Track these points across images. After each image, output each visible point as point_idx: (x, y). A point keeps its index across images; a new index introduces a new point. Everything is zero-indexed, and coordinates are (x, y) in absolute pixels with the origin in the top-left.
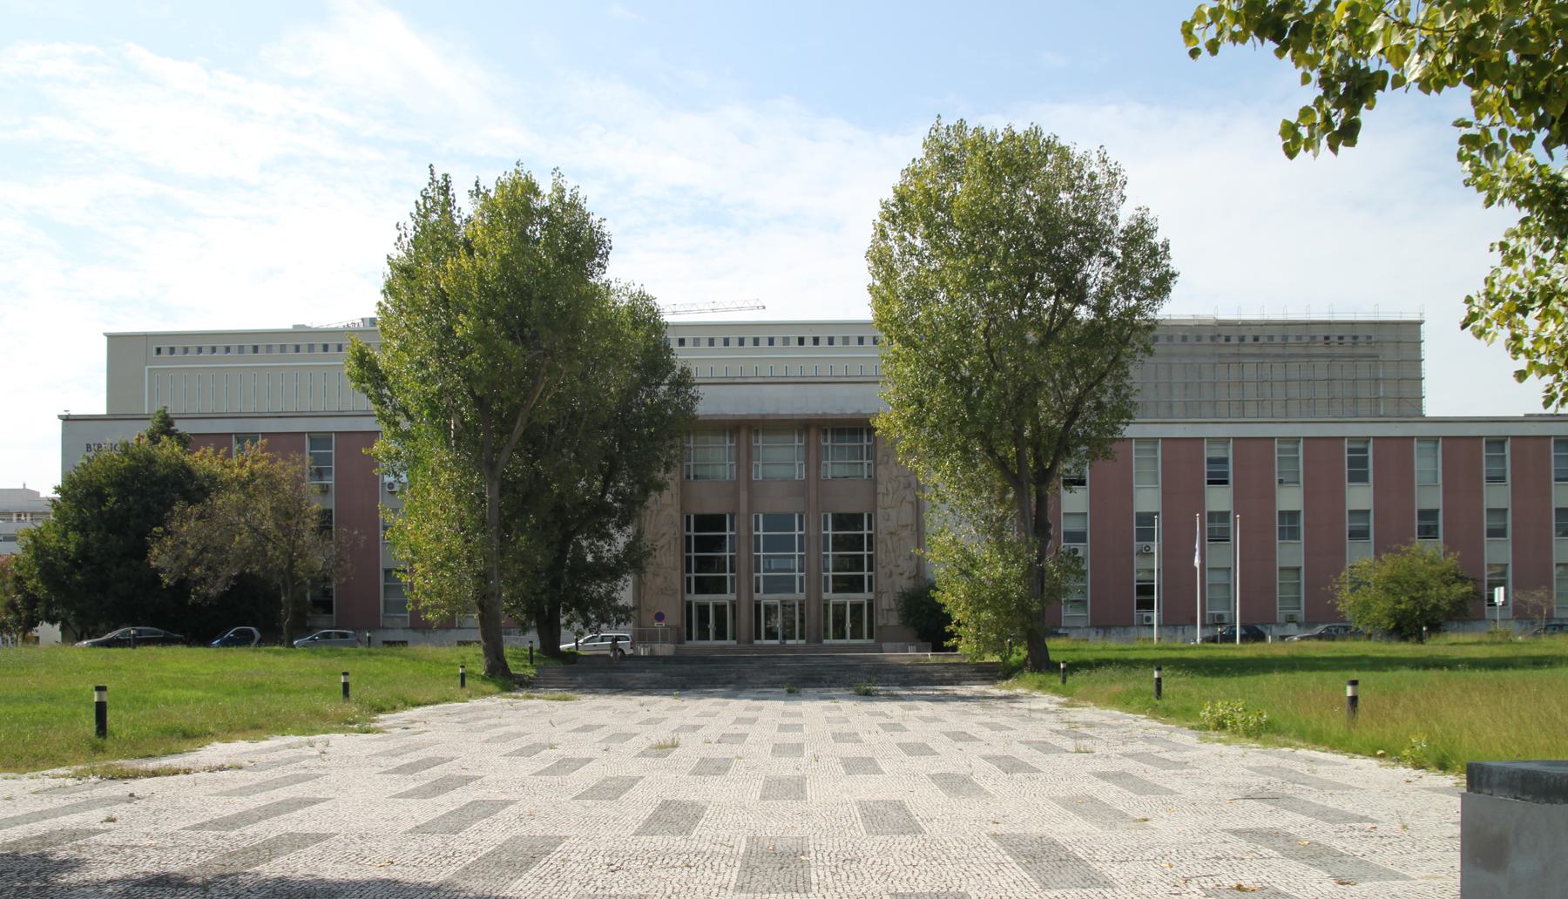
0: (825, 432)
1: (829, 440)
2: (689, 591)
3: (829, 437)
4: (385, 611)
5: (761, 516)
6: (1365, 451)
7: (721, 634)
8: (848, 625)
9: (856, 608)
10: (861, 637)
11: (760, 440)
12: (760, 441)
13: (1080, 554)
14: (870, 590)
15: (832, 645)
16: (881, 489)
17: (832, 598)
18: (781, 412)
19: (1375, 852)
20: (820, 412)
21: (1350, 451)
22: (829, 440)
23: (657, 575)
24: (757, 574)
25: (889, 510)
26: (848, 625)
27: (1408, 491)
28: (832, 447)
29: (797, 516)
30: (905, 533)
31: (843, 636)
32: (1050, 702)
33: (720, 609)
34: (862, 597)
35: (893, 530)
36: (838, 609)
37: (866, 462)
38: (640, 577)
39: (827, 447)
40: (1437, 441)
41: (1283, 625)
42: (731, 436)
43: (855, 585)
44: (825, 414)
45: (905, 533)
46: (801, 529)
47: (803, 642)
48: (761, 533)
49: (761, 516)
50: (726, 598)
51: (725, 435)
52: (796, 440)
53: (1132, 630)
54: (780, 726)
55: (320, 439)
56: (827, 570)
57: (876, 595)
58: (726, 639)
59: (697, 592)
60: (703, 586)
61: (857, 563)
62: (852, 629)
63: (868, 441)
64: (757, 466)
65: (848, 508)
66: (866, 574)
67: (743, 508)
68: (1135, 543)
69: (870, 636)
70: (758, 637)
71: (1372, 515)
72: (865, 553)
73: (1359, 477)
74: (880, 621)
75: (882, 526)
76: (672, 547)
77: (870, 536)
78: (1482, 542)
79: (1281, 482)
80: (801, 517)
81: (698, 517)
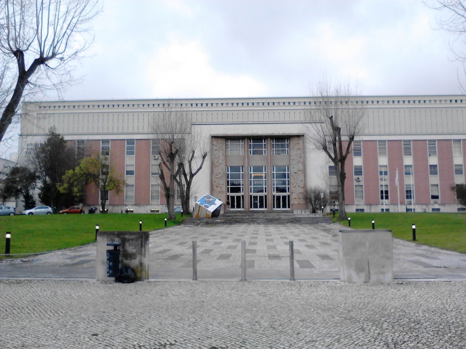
1: (274, 142)
2: (228, 192)
4: (126, 199)
5: (252, 167)
8: (236, 204)
9: (284, 198)
10: (286, 208)
13: (360, 180)
14: (289, 192)
15: (253, 211)
16: (292, 158)
19: (104, 312)
22: (274, 142)
24: (251, 186)
25: (295, 166)
26: (236, 204)
27: (450, 158)
28: (275, 144)
29: (241, 167)
30: (300, 173)
31: (279, 207)
33: (238, 198)
36: (278, 198)
37: (286, 149)
38: (305, 187)
39: (273, 144)
41: (433, 205)
42: (242, 141)
43: (284, 190)
45: (300, 173)
46: (242, 171)
48: (275, 172)
49: (252, 167)
50: (263, 194)
52: (286, 141)
53: (379, 206)
54: (257, 239)
55: (130, 142)
56: (274, 185)
57: (291, 193)
58: (240, 208)
59: (231, 192)
60: (233, 190)
61: (284, 183)
63: (265, 142)
64: (228, 151)
67: (246, 165)
68: (354, 176)
69: (289, 207)
70: (274, 207)
71: (388, 167)
72: (241, 179)
73: (408, 153)
74: (292, 202)
75: (293, 170)
76: (223, 177)
77: (288, 174)
78: (454, 176)
79: (430, 155)
80: (265, 167)
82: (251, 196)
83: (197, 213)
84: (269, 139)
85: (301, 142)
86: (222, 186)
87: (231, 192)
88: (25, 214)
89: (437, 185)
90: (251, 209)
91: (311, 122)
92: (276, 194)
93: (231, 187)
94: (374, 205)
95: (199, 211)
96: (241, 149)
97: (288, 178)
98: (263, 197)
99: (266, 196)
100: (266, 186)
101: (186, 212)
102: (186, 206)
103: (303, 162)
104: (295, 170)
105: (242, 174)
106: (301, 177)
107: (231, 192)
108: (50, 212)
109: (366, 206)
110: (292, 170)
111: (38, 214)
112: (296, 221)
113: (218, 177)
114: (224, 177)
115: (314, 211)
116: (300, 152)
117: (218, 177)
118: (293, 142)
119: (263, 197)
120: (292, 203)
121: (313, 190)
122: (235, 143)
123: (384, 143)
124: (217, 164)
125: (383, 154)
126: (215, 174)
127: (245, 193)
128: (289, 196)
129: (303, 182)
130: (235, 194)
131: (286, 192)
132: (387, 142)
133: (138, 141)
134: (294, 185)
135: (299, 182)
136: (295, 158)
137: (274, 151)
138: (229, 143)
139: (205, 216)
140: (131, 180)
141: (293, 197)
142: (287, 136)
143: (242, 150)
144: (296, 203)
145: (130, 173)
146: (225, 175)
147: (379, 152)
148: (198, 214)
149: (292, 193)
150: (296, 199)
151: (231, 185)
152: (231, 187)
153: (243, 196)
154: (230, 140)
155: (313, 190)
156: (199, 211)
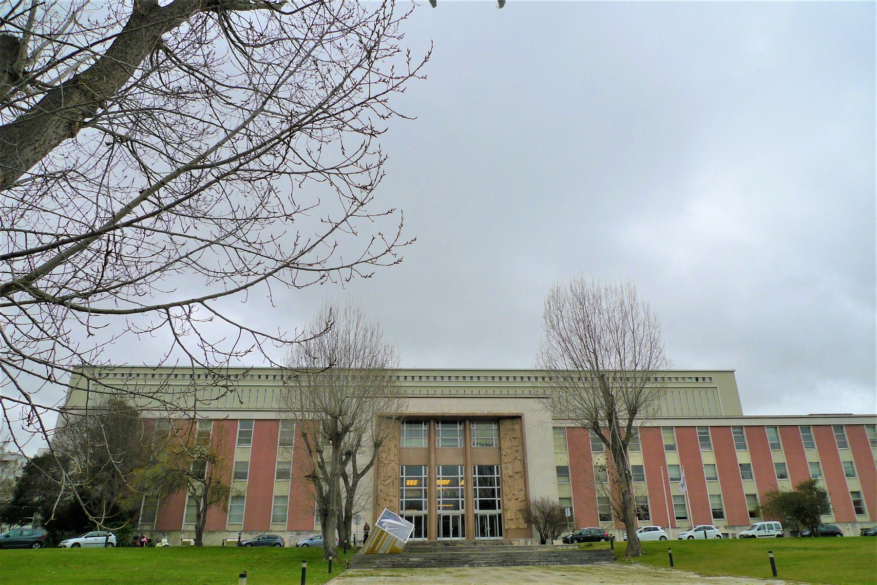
0: (438, 423)
2: (402, 509)
3: (440, 425)
6: (707, 433)
7: (455, 534)
9: (492, 518)
10: (420, 536)
11: (405, 427)
12: (474, 427)
16: (503, 453)
17: (480, 512)
18: (452, 412)
20: (471, 412)
21: (699, 433)
23: (386, 500)
25: (508, 464)
26: (451, 529)
32: (353, 572)
34: (462, 511)
35: (511, 475)
38: (527, 499)
40: (776, 428)
43: (489, 505)
44: (474, 413)
45: (517, 477)
46: (498, 474)
47: (464, 539)
51: (422, 424)
60: (484, 505)
62: (453, 531)
64: (438, 440)
65: (486, 462)
66: (497, 499)
74: (505, 526)
76: (394, 484)
80: (497, 467)
81: (444, 467)
82: (476, 516)
83: (371, 546)
84: (432, 423)
85: (517, 427)
86: (392, 498)
87: (480, 509)
88: (65, 546)
89: (570, 499)
90: (439, 539)
91: (540, 396)
92: (480, 512)
93: (406, 501)
94: (175, 531)
95: (378, 541)
96: (459, 438)
97: (498, 485)
98: (421, 517)
99: (463, 516)
100: (463, 499)
101: (345, 546)
102: (346, 532)
103: (521, 458)
104: (510, 472)
105: (497, 477)
106: (520, 484)
107: (480, 509)
108: (112, 544)
109: (617, 530)
110: (504, 471)
111: (90, 548)
112: (509, 560)
113: (387, 483)
114: (397, 484)
115: (543, 542)
116: (515, 443)
117: (387, 483)
118: (506, 425)
119: (421, 517)
120: (507, 527)
121: (551, 504)
122: (450, 428)
123: (739, 430)
124: (386, 462)
125: (742, 446)
126: (383, 479)
127: (430, 511)
128: (500, 515)
129: (523, 493)
130: (488, 512)
131: (496, 509)
132: (844, 428)
133: (259, 422)
134: (509, 497)
135: (516, 492)
136: (509, 453)
137: (440, 440)
138: (475, 428)
139: (388, 552)
140: (239, 486)
141: (508, 515)
142: (460, 417)
143: (461, 440)
144: (513, 527)
145: (241, 476)
146: (398, 480)
147: (805, 443)
148: (374, 546)
149: (504, 510)
150: (512, 521)
151: (406, 498)
152: (406, 501)
153: (426, 516)
154: (407, 423)
155: (551, 504)
156: (378, 541)
